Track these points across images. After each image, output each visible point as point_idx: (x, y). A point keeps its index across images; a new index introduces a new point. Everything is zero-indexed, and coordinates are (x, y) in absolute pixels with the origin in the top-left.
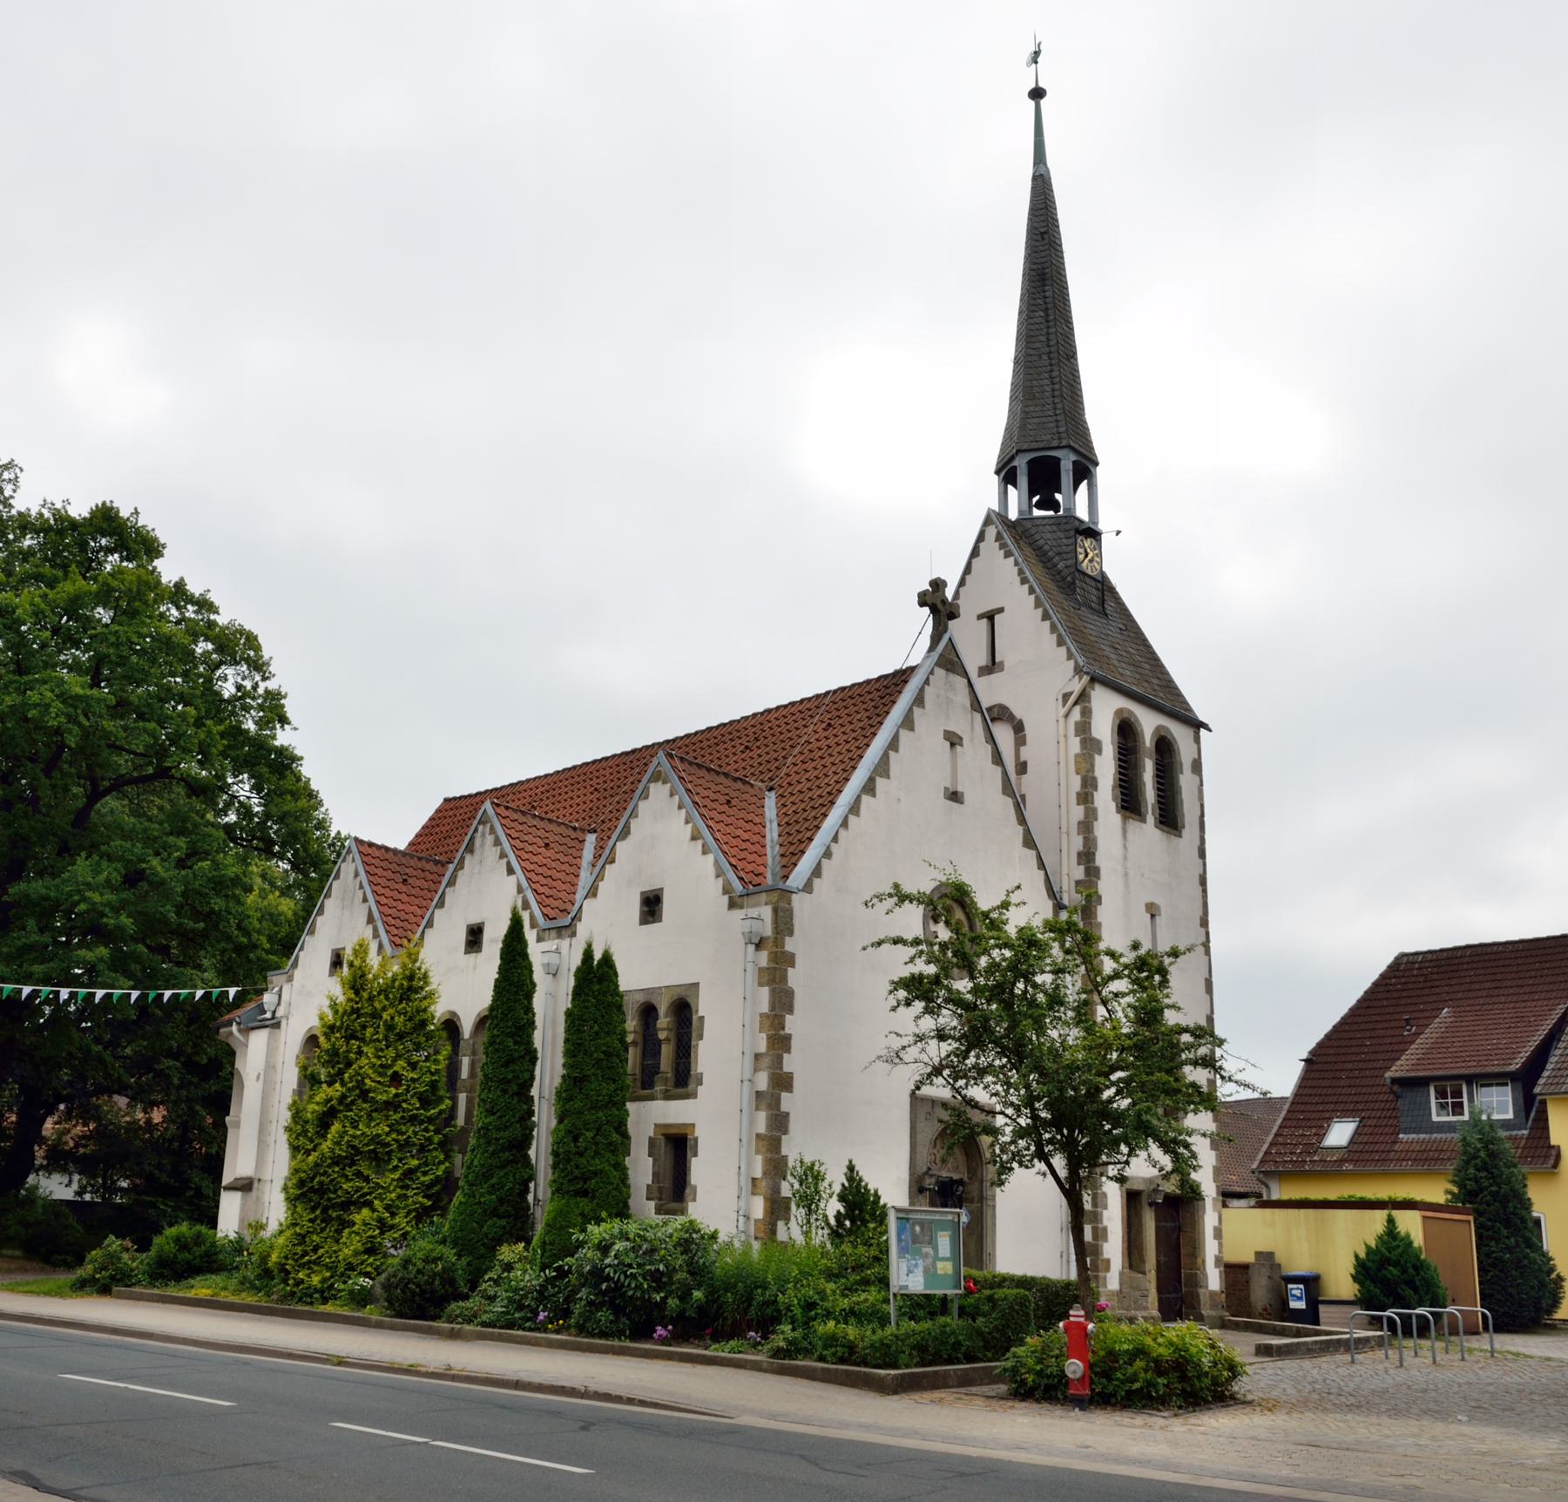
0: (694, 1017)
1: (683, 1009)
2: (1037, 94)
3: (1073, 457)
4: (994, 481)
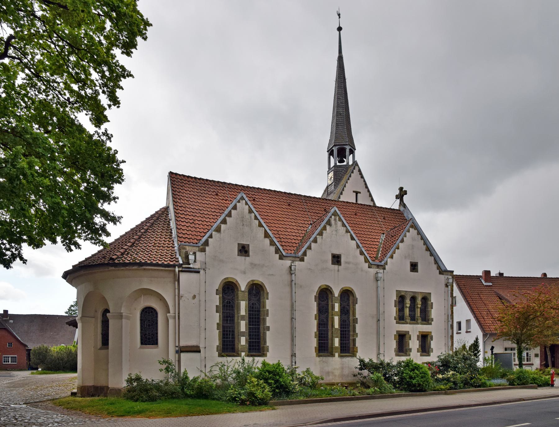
0: (429, 303)
1: (426, 299)
2: (340, 29)
3: (350, 147)
4: (327, 154)
